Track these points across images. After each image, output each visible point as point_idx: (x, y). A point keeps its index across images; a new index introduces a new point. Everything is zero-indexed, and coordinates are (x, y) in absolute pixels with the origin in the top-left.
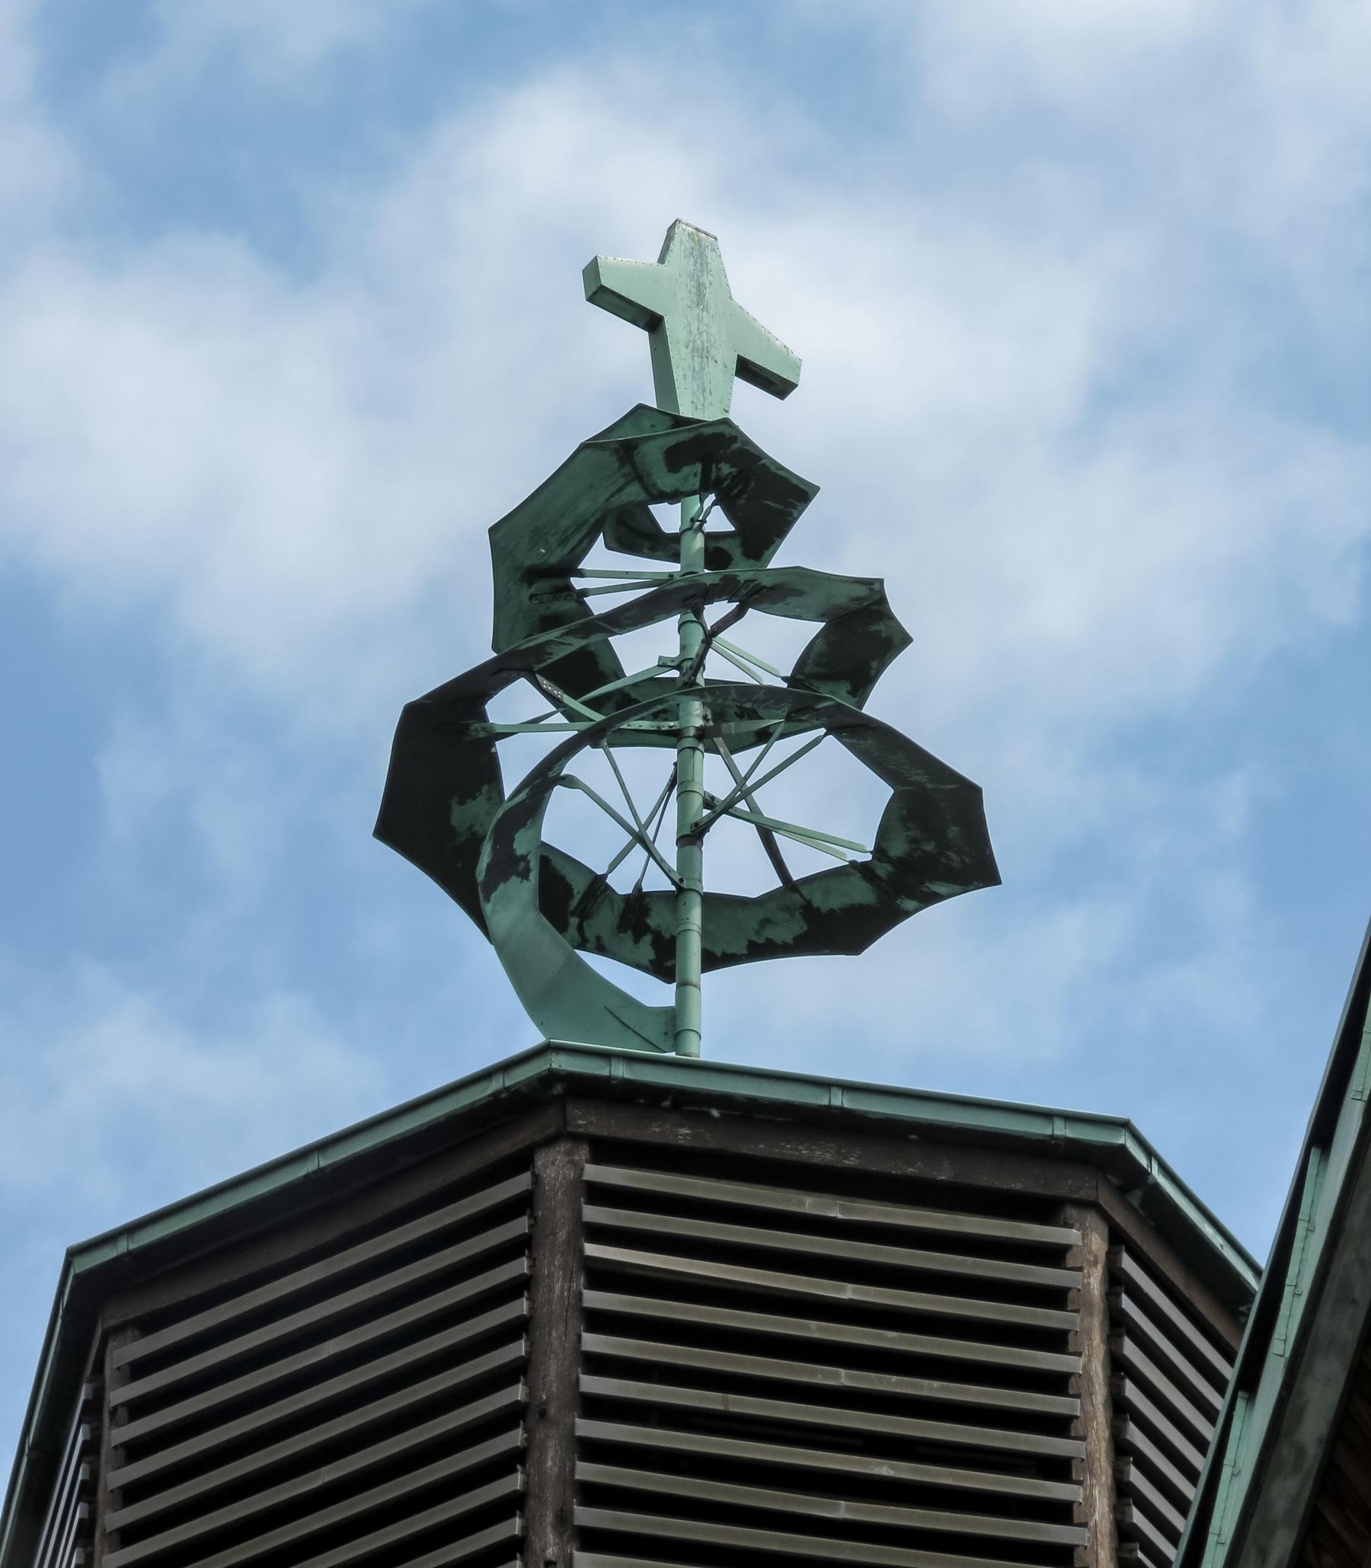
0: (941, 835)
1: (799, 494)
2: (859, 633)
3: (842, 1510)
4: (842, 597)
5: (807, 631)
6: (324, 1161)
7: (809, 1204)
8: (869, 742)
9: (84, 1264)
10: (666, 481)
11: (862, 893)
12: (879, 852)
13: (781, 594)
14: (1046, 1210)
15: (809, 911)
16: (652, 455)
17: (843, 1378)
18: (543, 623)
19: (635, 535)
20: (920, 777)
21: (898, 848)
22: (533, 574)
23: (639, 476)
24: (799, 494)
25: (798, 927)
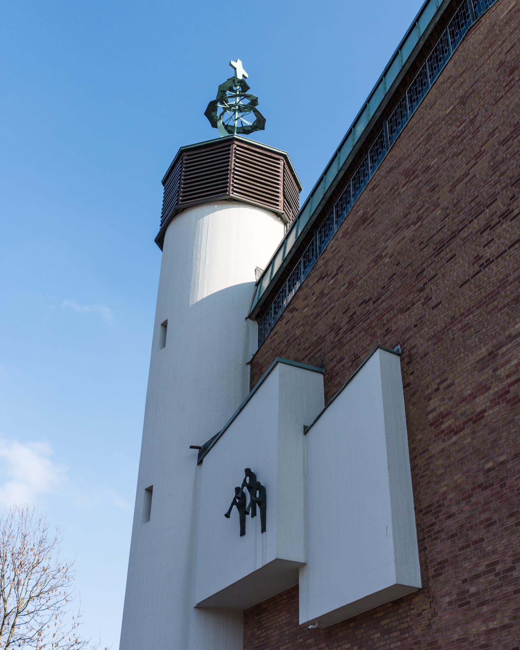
0: (260, 124)
1: (248, 88)
2: (254, 102)
3: (258, 185)
4: (254, 98)
5: (249, 101)
6: (187, 148)
7: (257, 155)
8: (256, 113)
9: (182, 149)
10: (237, 84)
11: (250, 129)
12: (253, 125)
13: (246, 96)
14: (278, 159)
15: (244, 130)
16: (236, 81)
17: (259, 172)
18: (222, 98)
19: (231, 89)
20: (260, 118)
21: (255, 125)
22: (222, 91)
23: (234, 83)
24: (248, 88)
25: (242, 131)
